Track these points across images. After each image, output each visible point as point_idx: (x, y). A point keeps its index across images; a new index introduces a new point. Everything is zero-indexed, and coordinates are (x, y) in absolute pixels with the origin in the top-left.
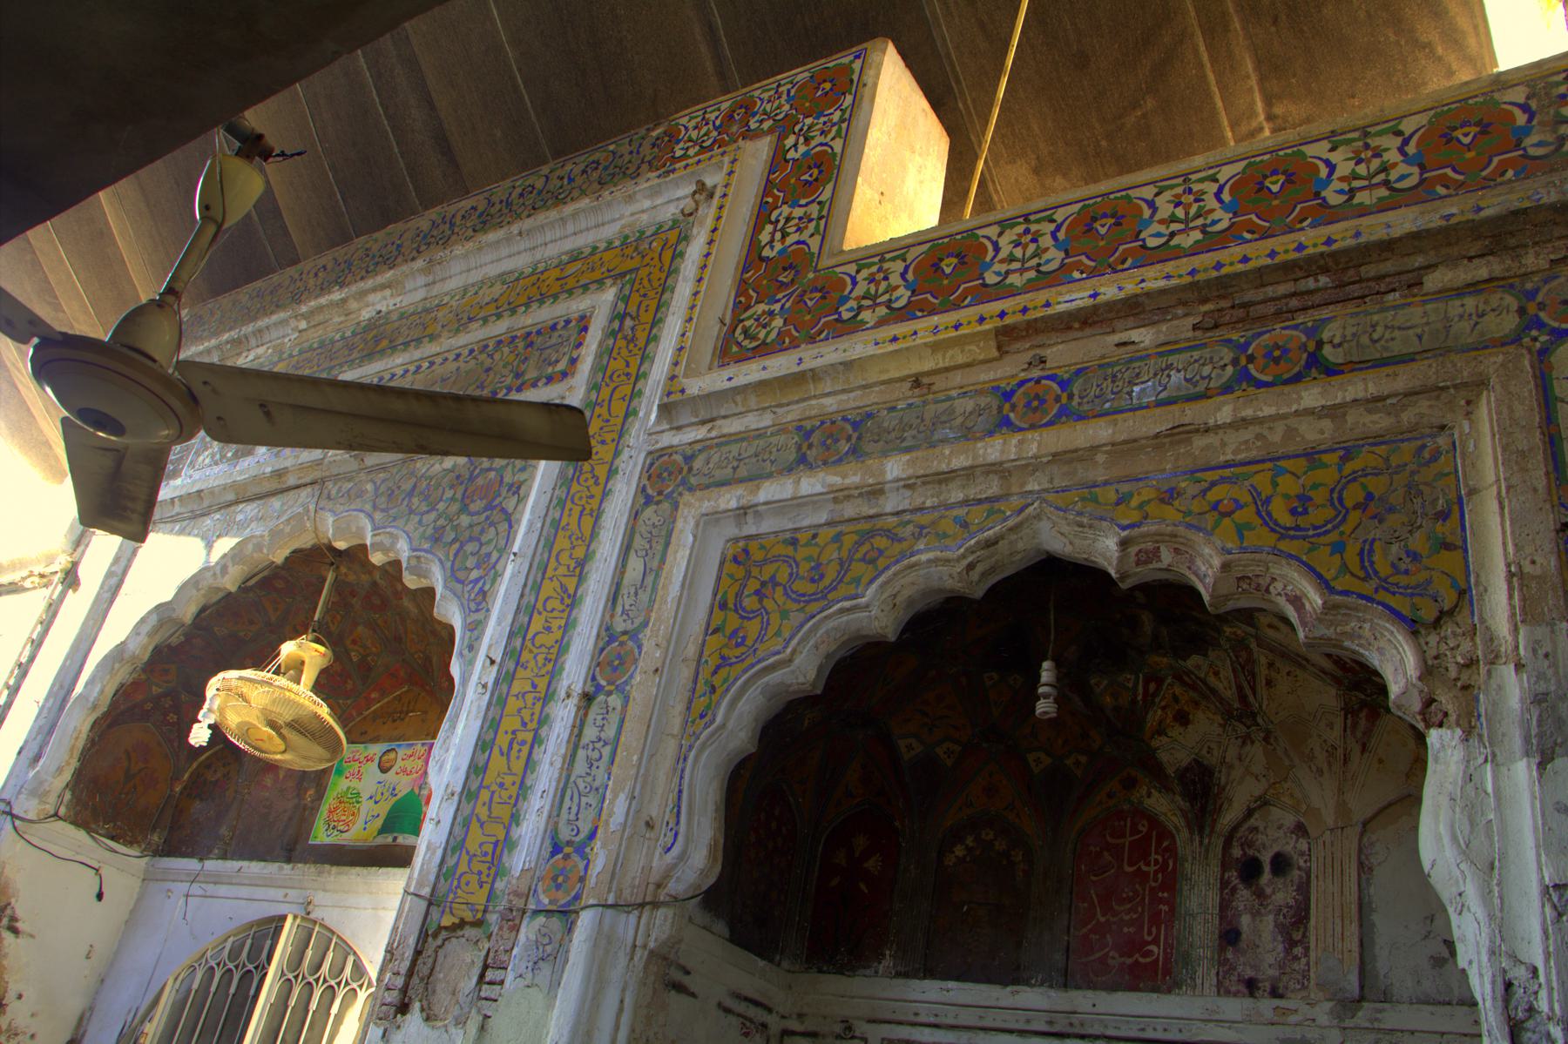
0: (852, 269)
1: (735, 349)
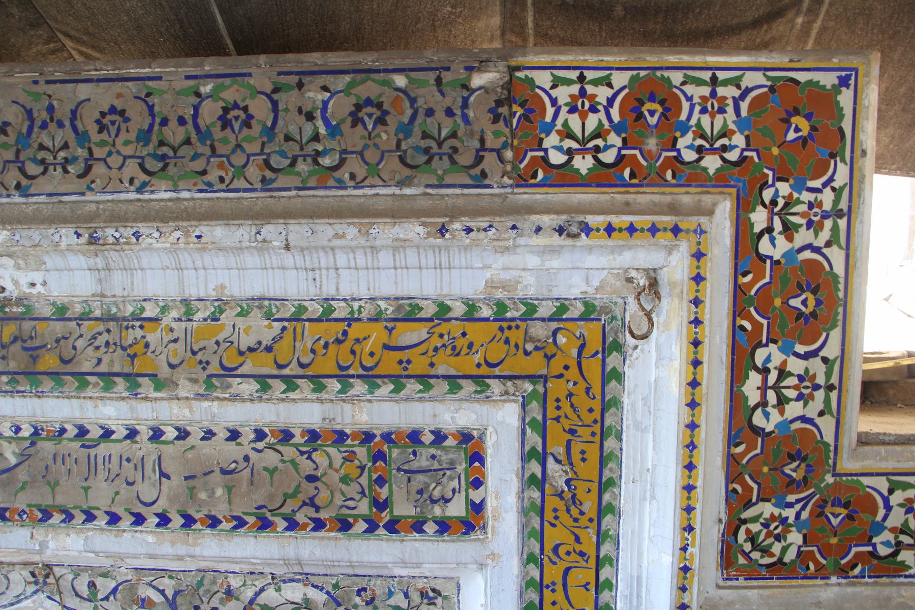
0: (882, 484)
1: (742, 560)
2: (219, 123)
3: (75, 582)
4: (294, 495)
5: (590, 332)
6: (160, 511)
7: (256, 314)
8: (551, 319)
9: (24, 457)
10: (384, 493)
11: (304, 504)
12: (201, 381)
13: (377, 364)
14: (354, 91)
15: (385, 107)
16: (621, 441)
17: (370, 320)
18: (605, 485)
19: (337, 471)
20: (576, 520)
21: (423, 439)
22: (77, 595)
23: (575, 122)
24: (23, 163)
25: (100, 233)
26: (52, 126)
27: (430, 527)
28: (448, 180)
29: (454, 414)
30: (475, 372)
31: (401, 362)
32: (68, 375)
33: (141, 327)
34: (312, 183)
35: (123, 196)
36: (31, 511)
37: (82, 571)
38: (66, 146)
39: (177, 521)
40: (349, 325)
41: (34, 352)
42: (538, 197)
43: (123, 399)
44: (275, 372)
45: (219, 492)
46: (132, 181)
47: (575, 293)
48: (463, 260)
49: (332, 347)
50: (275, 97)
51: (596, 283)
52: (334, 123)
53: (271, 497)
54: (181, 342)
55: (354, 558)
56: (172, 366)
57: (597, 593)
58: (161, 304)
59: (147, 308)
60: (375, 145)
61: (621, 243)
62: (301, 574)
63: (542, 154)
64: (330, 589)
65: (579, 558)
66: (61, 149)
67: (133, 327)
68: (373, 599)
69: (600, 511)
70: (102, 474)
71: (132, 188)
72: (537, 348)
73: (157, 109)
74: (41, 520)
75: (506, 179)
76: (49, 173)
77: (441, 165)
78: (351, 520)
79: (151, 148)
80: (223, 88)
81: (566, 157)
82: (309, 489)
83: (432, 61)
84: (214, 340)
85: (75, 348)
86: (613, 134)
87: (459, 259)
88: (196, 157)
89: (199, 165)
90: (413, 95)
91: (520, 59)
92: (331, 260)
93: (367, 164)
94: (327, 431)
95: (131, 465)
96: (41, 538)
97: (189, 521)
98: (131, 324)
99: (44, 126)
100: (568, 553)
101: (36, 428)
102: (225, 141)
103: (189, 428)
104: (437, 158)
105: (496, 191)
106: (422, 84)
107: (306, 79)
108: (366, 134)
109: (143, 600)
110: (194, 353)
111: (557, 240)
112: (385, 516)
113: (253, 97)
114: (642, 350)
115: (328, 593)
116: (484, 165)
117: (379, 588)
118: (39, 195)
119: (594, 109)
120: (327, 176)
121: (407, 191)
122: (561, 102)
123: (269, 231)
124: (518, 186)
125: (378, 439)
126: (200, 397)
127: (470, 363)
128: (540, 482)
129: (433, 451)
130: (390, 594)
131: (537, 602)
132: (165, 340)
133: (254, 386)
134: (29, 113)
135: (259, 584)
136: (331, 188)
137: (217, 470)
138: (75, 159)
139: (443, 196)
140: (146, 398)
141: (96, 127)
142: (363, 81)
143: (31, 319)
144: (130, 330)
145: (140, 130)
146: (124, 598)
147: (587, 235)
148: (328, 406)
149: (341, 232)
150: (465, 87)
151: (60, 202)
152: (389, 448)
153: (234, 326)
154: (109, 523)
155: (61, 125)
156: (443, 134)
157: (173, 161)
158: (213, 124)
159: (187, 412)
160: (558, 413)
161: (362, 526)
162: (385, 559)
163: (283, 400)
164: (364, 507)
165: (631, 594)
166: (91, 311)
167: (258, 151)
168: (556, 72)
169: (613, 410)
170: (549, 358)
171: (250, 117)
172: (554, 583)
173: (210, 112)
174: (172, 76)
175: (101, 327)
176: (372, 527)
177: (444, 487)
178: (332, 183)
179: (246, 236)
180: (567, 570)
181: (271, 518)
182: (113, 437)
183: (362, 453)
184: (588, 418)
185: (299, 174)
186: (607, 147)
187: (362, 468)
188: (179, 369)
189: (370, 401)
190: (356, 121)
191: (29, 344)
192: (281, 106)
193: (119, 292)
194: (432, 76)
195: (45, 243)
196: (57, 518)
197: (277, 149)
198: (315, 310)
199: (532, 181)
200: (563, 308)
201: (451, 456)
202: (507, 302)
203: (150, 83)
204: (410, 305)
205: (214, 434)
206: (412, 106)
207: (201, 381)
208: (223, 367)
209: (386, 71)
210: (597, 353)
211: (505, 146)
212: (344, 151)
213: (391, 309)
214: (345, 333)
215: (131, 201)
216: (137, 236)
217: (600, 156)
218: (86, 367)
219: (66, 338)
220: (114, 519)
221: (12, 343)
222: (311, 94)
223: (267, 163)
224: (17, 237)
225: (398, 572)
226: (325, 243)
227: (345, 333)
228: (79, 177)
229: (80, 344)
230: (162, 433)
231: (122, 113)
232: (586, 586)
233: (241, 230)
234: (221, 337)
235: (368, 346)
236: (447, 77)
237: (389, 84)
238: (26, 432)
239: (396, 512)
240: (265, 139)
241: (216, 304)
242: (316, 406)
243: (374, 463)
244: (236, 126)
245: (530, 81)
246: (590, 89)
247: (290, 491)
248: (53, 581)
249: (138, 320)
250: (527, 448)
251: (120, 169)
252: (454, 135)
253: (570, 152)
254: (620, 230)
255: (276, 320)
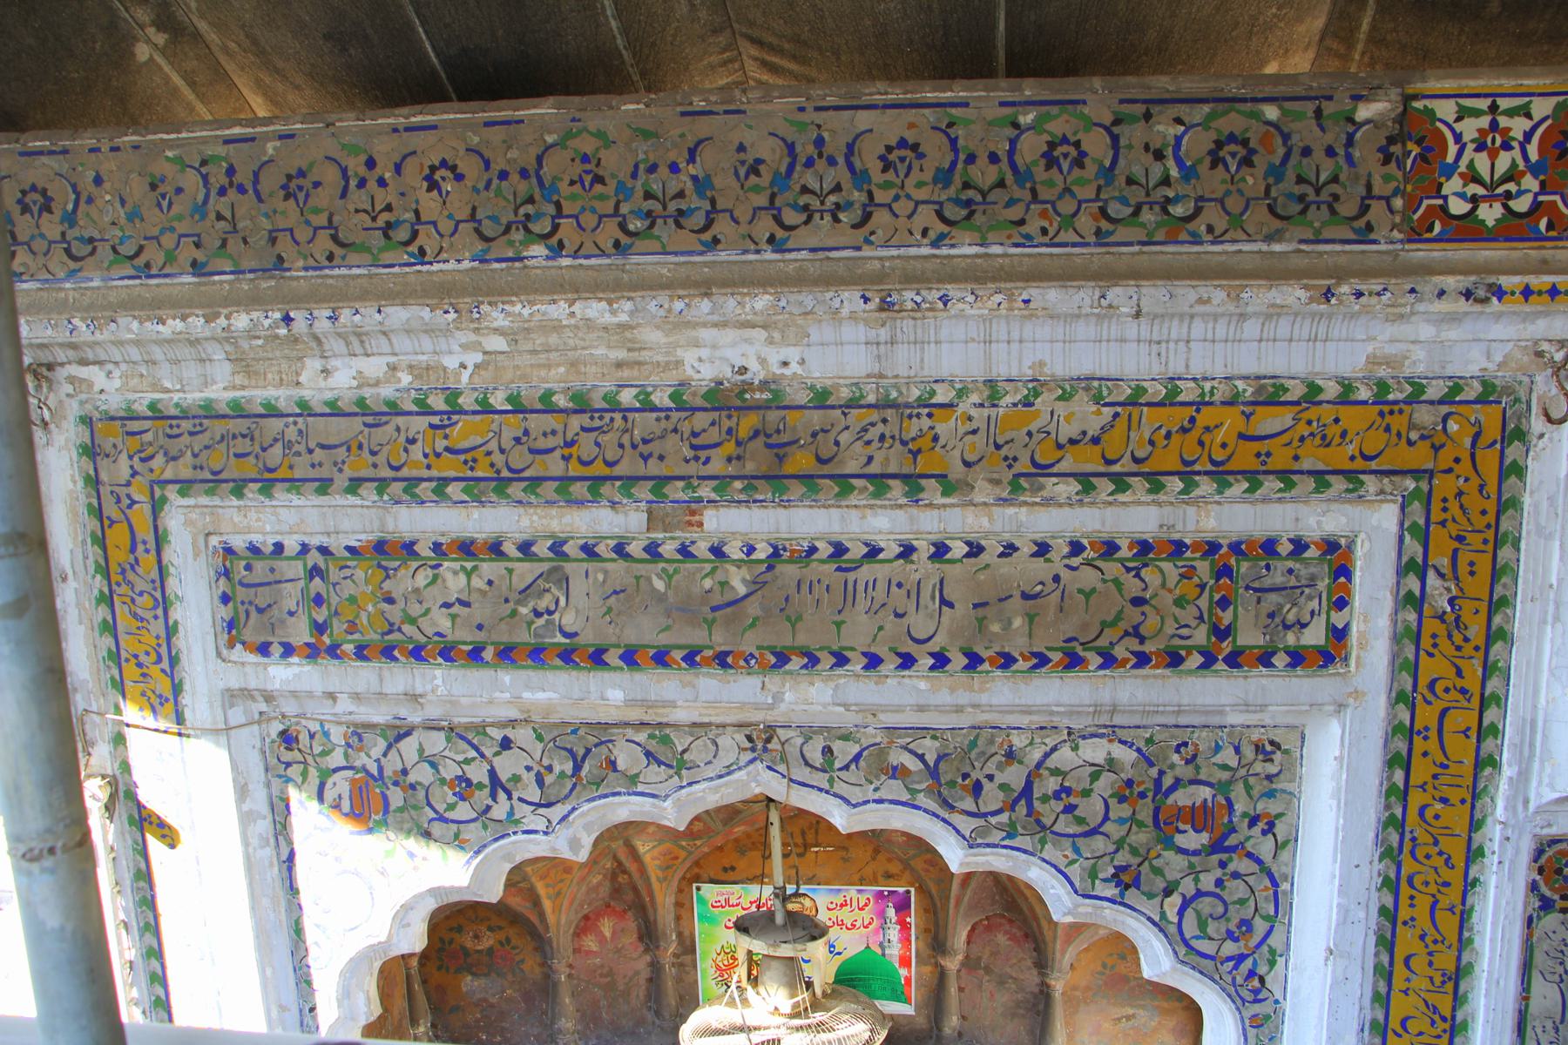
2: (1043, 162)
3: (805, 748)
4: (1113, 624)
5: (1489, 417)
6: (937, 649)
7: (1082, 396)
8: (1441, 402)
9: (757, 585)
10: (1226, 617)
11: (1127, 633)
12: (1005, 481)
13: (1230, 458)
14: (1213, 125)
15: (1252, 145)
16: (1518, 550)
17: (1223, 403)
18: (1498, 604)
19: (1170, 591)
20: (1459, 648)
21: (1279, 549)
22: (807, 764)
23: (1482, 163)
24: (779, 210)
25: (895, 297)
26: (821, 165)
27: (1280, 660)
28: (1326, 234)
29: (1319, 517)
30: (1348, 466)
31: (1258, 455)
32: (827, 478)
33: (930, 415)
34: (1159, 236)
35: (913, 251)
36: (762, 655)
37: (815, 733)
38: (838, 188)
39: (959, 661)
40: (1198, 411)
41: (780, 451)
42: (1435, 254)
43: (901, 506)
44: (1102, 469)
45: (1017, 622)
46: (925, 233)
47: (1474, 369)
48: (1344, 331)
49: (1175, 438)
50: (1116, 130)
51: (1498, 358)
52: (1189, 164)
53: (1085, 626)
54: (982, 434)
55: (1185, 701)
56: (967, 464)
57: (1478, 741)
58: (958, 386)
59: (939, 391)
60: (1239, 191)
61: (1540, 308)
62: (1106, 727)
63: (1440, 202)
64: (1142, 744)
65: (1459, 696)
66: (831, 192)
67: (918, 416)
68: (1195, 756)
69: (1488, 637)
70: (862, 603)
71: (925, 241)
72: (1423, 437)
73: (961, 143)
74: (774, 666)
75: (1395, 233)
76: (813, 222)
77: (1317, 216)
78: (1183, 653)
79: (952, 191)
80: (1051, 118)
81: (1470, 206)
82: (1134, 614)
83: (1311, 88)
84: (1025, 430)
85: (837, 443)
86: (1528, 177)
87: (1339, 329)
88: (1011, 203)
89: (1015, 213)
90: (1286, 130)
91: (1419, 85)
92: (1185, 330)
93: (1228, 214)
94: (1161, 542)
95: (903, 591)
96: (774, 689)
97: (974, 661)
98: (915, 411)
99: (810, 163)
100: (1447, 690)
101: (775, 548)
102: (1050, 183)
103: (983, 543)
104: (1314, 207)
105: (1383, 247)
106: (1298, 116)
107: (1155, 109)
108: (1228, 177)
109: (895, 768)
110: (998, 447)
111: (1463, 305)
112: (1226, 647)
113: (1087, 130)
114: (1551, 439)
115: (1139, 750)
116: (716, 229)
117: (1203, 740)
118: (799, 250)
119: (1506, 146)
120: (1177, 228)
121: (1277, 247)
122: (1466, 138)
123: (1116, 294)
124: (1410, 241)
125: (1224, 550)
126: (1003, 502)
127: (1341, 455)
128: (1417, 601)
129: (1290, 564)
130: (1218, 749)
131: (1404, 753)
132: (961, 431)
133: (1073, 487)
134: (791, 148)
135: (1050, 742)
136: (1182, 243)
137: (1017, 594)
138: (850, 204)
139: (1321, 254)
140: (930, 505)
141: (880, 165)
142: (1225, 113)
143: (778, 408)
144: (914, 419)
145: (938, 169)
146: (869, 766)
147: (1500, 300)
148: (1167, 509)
149: (1205, 296)
150: (1351, 120)
151: (828, 258)
152: (1237, 562)
153: (1052, 413)
154: (866, 668)
155: (832, 162)
156: (1323, 178)
157: (981, 208)
158: (1035, 162)
159: (985, 522)
160: (1443, 516)
161: (1196, 660)
162: (1223, 701)
163: (1110, 503)
164: (1201, 636)
165: (1522, 742)
166: (862, 397)
167: (1093, 196)
168: (1461, 101)
169: (1510, 512)
170: (1436, 449)
171: (1083, 154)
172: (1427, 729)
173: (1031, 148)
174: (981, 104)
175: (875, 416)
176: (1209, 661)
177: (1301, 609)
178: (1183, 236)
179: (1088, 301)
180: (1444, 712)
181: (1082, 654)
182: (881, 556)
183: (1204, 568)
184: (1480, 522)
185: (1143, 225)
186: (1520, 193)
187: (1202, 587)
188: (977, 468)
189: (1219, 503)
190: (1216, 161)
191: (774, 440)
192: (1123, 142)
193: (903, 371)
194: (1310, 107)
195: (819, 310)
196: (796, 663)
197: (1117, 194)
198: (1157, 391)
199: (1427, 235)
200: (1456, 389)
201: (1312, 570)
202: (1390, 382)
203: (953, 111)
204: (1274, 385)
205: (1016, 549)
206: (1285, 143)
207: (1005, 481)
208: (1034, 464)
209: (1255, 100)
210: (1495, 442)
211: (1396, 192)
212: (1201, 199)
213: (1250, 390)
214: (1192, 420)
215: (925, 257)
216: (945, 300)
217: (1511, 203)
218: (852, 467)
219: (826, 431)
220: (873, 662)
221: (751, 439)
222: (1161, 128)
223: (1103, 212)
224: (783, 303)
225: (1235, 718)
226: (1186, 309)
227: (1192, 420)
228: (854, 227)
229: (844, 438)
230: (947, 549)
231: (915, 147)
232: (1465, 733)
233: (1082, 294)
234: (1033, 427)
235: (1220, 436)
236: (1329, 108)
237: (1257, 116)
238: (762, 552)
239: (1240, 642)
240: (1102, 182)
241: (1030, 385)
242: (1154, 510)
243: (1217, 580)
244: (1065, 166)
245: (1430, 113)
246: (1503, 122)
247: (1109, 619)
248: (779, 747)
249: (926, 406)
250: (1405, 559)
251: (910, 217)
252: (1335, 179)
253: (1475, 200)
254: (1540, 293)
255: (1106, 405)
